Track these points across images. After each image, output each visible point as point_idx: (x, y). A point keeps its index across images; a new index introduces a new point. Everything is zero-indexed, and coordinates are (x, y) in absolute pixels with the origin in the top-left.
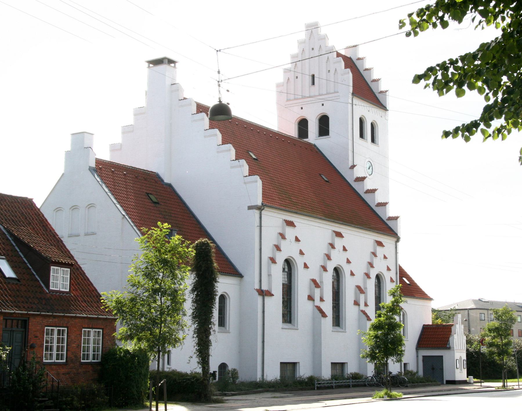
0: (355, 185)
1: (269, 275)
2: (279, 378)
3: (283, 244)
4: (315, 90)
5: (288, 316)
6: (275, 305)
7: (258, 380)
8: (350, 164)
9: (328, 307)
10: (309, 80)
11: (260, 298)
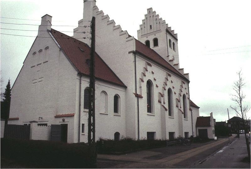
0: (170, 63)
1: (141, 87)
2: (146, 139)
3: (146, 74)
4: (152, 31)
5: (150, 109)
6: (143, 102)
7: (136, 140)
8: (167, 55)
9: (166, 106)
10: (149, 27)
11: (136, 99)
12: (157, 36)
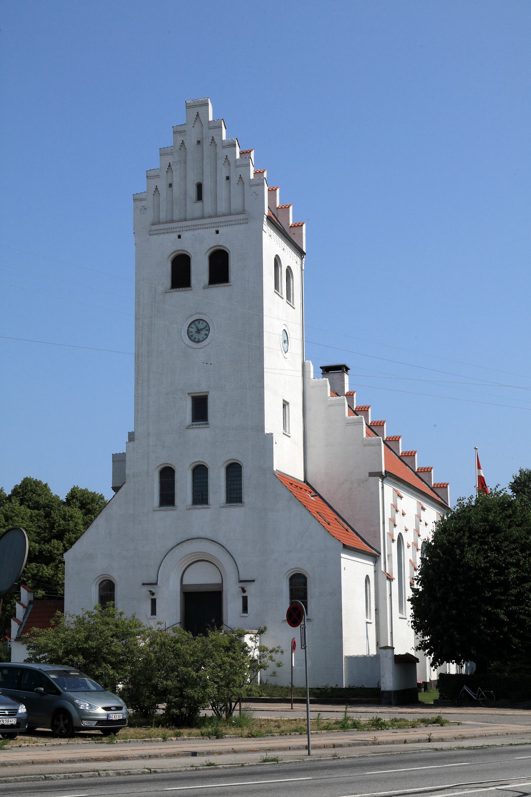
10: (192, 192)
12: (229, 239)
